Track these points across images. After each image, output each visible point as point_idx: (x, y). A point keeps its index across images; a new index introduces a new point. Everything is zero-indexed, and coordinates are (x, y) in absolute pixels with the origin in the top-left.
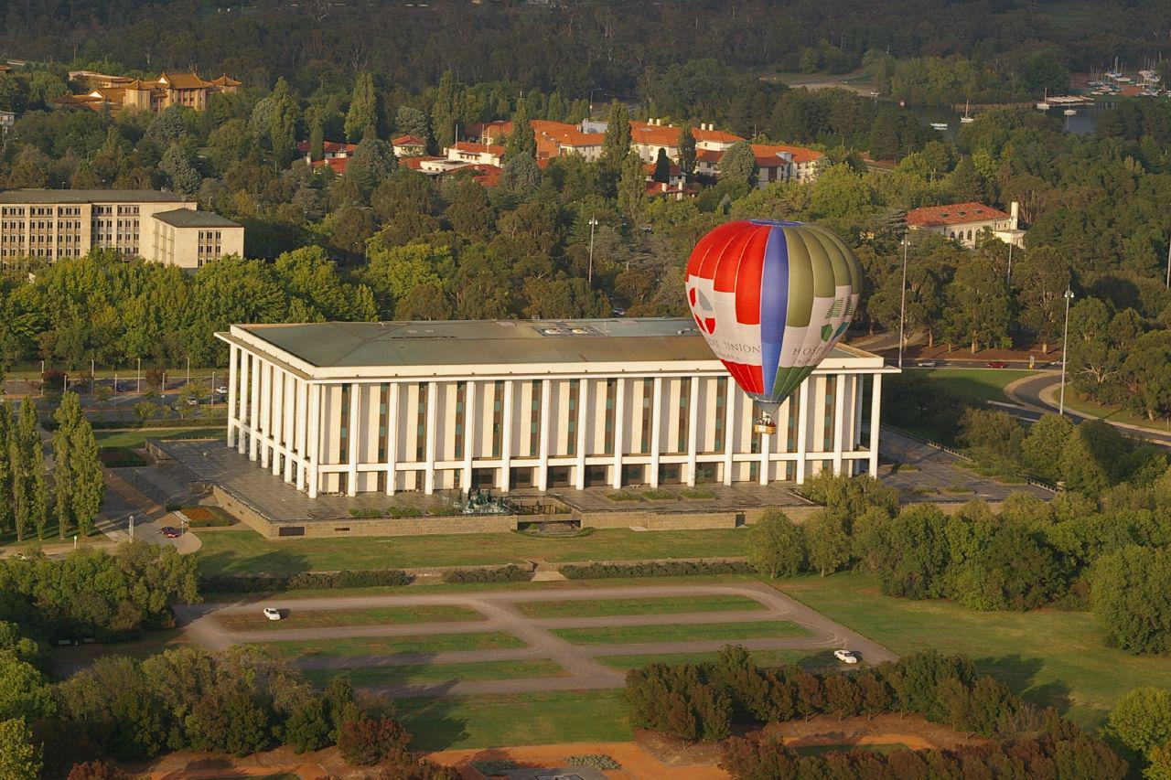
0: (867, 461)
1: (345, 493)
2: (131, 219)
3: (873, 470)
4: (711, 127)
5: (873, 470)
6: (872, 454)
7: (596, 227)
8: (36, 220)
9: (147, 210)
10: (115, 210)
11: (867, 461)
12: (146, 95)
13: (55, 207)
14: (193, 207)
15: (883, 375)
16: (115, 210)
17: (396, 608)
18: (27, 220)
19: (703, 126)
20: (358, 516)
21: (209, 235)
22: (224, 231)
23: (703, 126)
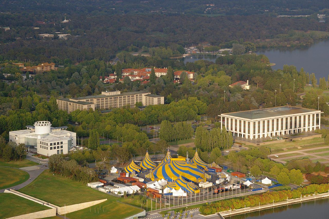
0: (319, 127)
1: (255, 138)
2: (141, 96)
3: (320, 128)
4: (166, 68)
5: (320, 128)
6: (319, 126)
7: (225, 92)
8: (110, 100)
9: (143, 95)
10: (139, 95)
11: (319, 127)
12: (41, 68)
13: (90, 99)
14: (150, 93)
15: (321, 114)
16: (139, 95)
17: (307, 149)
18: (113, 99)
19: (165, 68)
20: (264, 141)
21: (89, 106)
22: (161, 97)
23: (165, 68)
